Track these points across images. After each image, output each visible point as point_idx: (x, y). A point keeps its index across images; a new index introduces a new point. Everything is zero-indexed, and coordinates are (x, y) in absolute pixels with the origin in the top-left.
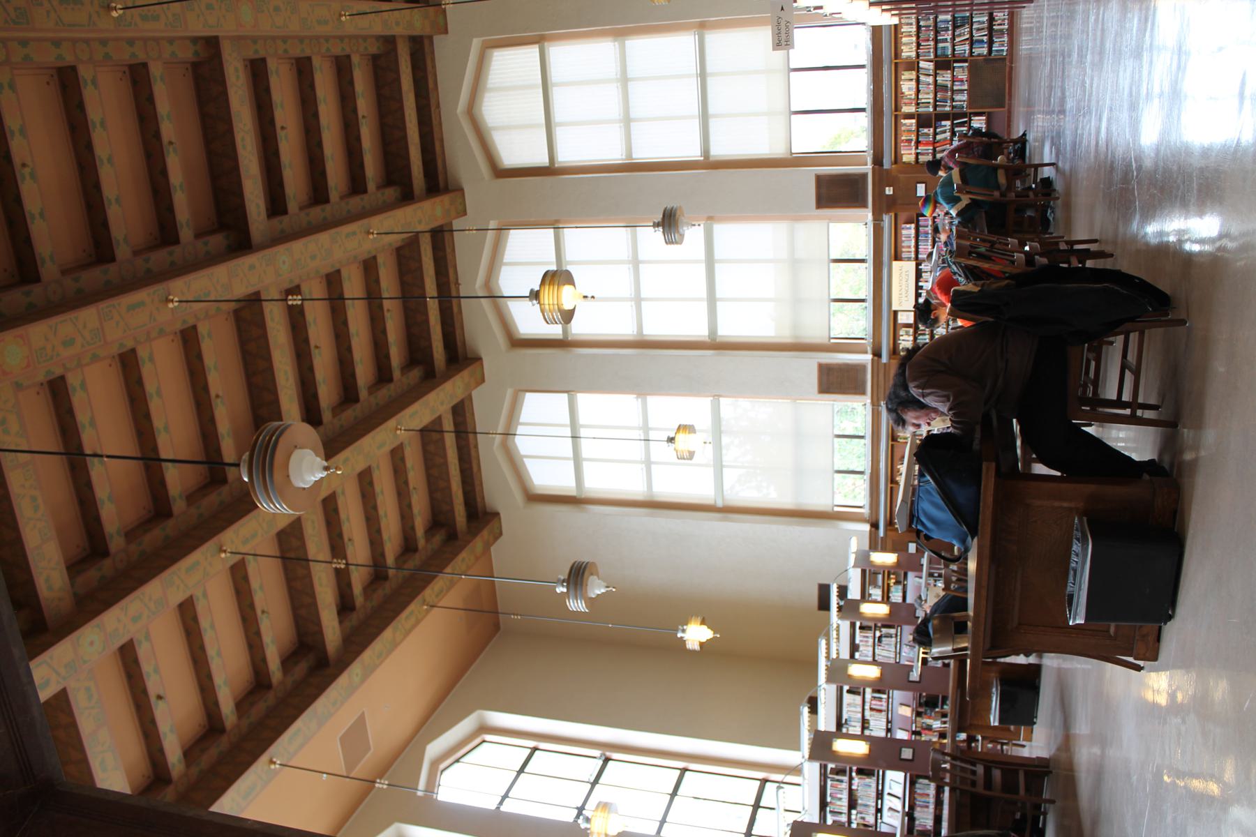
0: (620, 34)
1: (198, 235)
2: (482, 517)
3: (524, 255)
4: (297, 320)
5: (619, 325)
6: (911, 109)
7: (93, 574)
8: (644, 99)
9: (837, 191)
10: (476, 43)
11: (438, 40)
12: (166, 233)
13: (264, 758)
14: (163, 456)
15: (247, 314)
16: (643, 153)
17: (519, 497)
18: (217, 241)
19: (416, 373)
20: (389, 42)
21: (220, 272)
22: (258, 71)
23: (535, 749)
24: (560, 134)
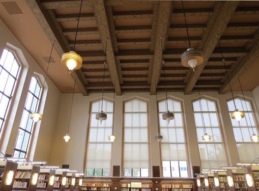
0: (148, 127)
1: (118, 46)
2: (89, 92)
3: (174, 106)
4: (101, 62)
5: (128, 123)
6: (173, 187)
7: (52, 14)
8: (136, 131)
9: (116, 170)
10: (148, 100)
11: (149, 93)
12: (119, 40)
13: (56, 39)
14: (78, 33)
15: (102, 53)
16: (126, 130)
17: (91, 100)
18: (117, 49)
19: (87, 83)
20: (150, 85)
21: (111, 49)
22: (147, 61)
23: (38, 99)
24: (130, 115)
